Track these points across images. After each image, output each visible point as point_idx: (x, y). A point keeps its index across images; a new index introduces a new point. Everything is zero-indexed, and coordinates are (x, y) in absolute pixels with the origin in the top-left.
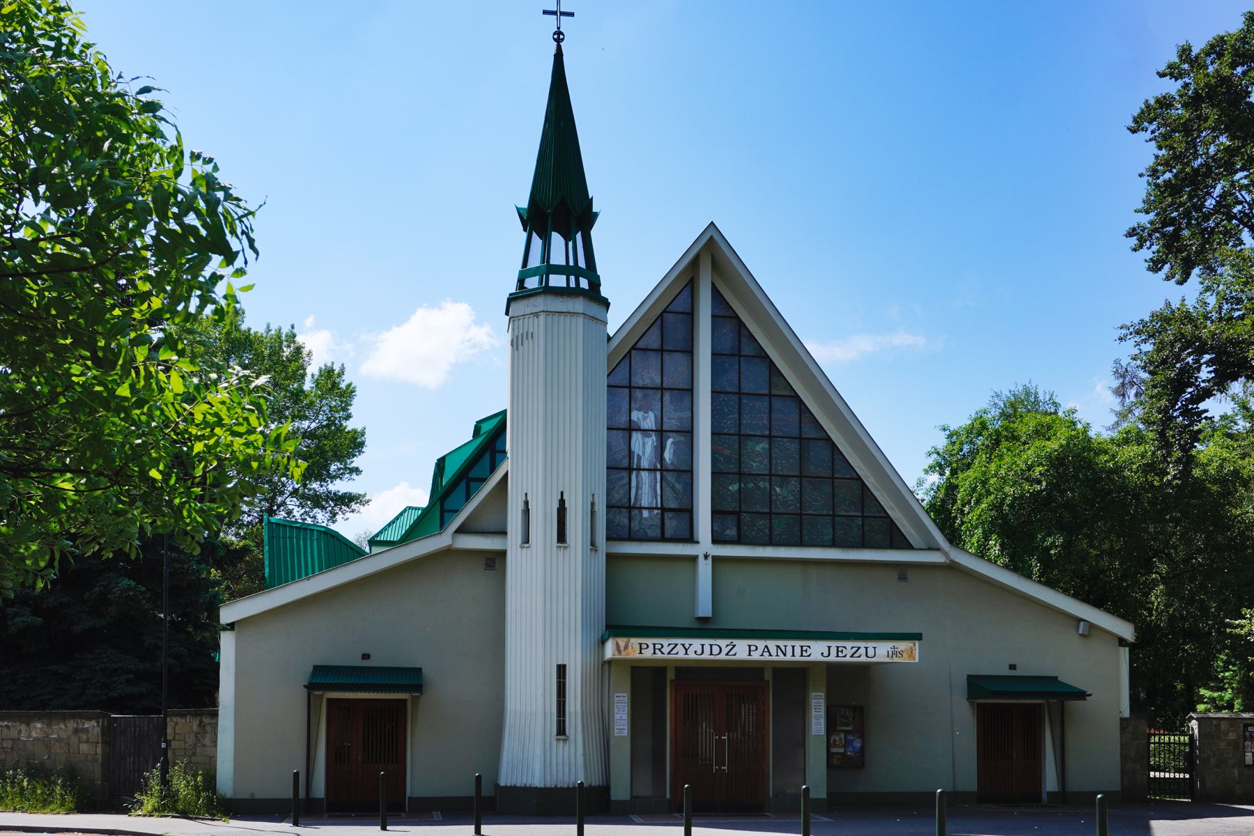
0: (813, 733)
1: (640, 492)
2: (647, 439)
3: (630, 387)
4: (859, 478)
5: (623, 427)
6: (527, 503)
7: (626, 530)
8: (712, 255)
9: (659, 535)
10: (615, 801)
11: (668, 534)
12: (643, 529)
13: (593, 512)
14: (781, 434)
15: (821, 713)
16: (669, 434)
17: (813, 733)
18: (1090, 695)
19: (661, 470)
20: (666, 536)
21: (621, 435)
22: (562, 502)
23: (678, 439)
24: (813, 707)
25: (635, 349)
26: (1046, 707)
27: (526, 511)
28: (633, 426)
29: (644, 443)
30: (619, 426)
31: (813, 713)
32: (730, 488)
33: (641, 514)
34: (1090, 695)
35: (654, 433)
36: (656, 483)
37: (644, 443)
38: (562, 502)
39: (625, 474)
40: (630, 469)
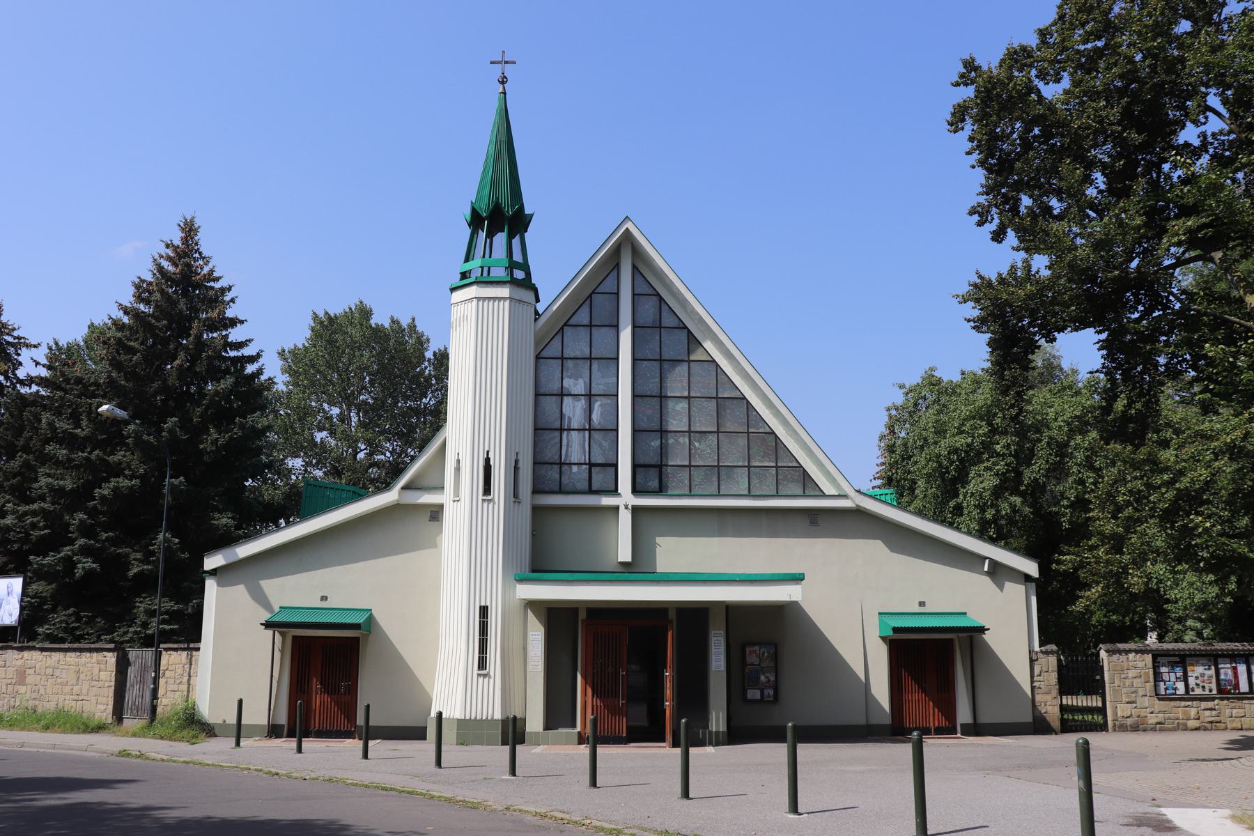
0: (713, 669)
1: (570, 449)
2: (576, 403)
3: (562, 358)
4: (773, 433)
5: (555, 392)
6: (458, 461)
7: (557, 483)
8: (632, 243)
9: (587, 488)
10: (372, 726)
11: (595, 487)
12: (573, 483)
13: (516, 468)
14: (698, 395)
15: (720, 650)
16: (596, 397)
17: (713, 669)
18: (988, 629)
19: (590, 430)
20: (593, 489)
21: (554, 400)
22: (487, 460)
23: (606, 402)
24: (713, 644)
25: (569, 325)
26: (957, 640)
27: (458, 469)
28: (564, 392)
29: (574, 407)
30: (551, 393)
31: (713, 650)
32: (652, 444)
33: (571, 469)
34: (988, 629)
35: (583, 397)
36: (584, 441)
37: (574, 407)
38: (487, 460)
39: (557, 434)
40: (561, 430)
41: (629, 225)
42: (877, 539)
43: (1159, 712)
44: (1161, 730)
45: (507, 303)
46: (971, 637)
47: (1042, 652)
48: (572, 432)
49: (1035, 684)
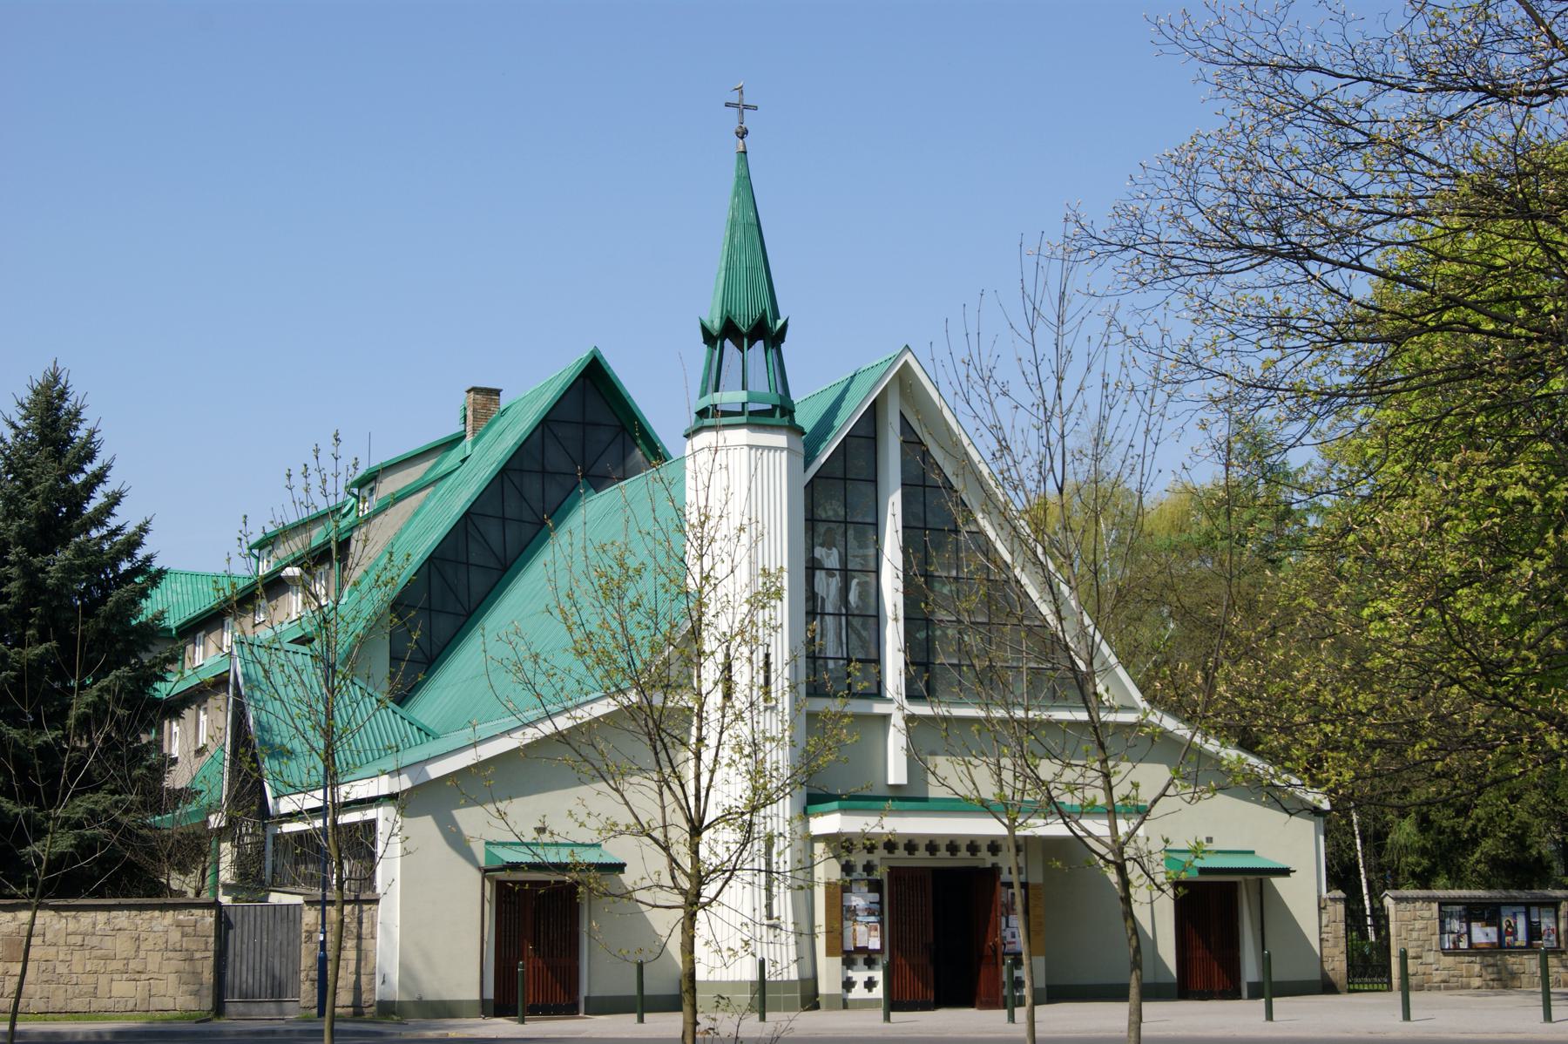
29: (828, 585)
36: (841, 630)
37: (828, 585)
41: (908, 357)
42: (1160, 762)
43: (1444, 969)
44: (1447, 988)
45: (785, 454)
46: (1261, 880)
47: (1331, 899)
48: (827, 617)
49: (1324, 936)
